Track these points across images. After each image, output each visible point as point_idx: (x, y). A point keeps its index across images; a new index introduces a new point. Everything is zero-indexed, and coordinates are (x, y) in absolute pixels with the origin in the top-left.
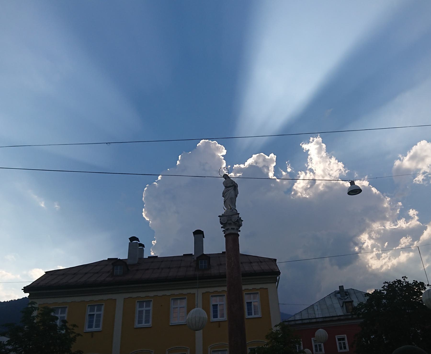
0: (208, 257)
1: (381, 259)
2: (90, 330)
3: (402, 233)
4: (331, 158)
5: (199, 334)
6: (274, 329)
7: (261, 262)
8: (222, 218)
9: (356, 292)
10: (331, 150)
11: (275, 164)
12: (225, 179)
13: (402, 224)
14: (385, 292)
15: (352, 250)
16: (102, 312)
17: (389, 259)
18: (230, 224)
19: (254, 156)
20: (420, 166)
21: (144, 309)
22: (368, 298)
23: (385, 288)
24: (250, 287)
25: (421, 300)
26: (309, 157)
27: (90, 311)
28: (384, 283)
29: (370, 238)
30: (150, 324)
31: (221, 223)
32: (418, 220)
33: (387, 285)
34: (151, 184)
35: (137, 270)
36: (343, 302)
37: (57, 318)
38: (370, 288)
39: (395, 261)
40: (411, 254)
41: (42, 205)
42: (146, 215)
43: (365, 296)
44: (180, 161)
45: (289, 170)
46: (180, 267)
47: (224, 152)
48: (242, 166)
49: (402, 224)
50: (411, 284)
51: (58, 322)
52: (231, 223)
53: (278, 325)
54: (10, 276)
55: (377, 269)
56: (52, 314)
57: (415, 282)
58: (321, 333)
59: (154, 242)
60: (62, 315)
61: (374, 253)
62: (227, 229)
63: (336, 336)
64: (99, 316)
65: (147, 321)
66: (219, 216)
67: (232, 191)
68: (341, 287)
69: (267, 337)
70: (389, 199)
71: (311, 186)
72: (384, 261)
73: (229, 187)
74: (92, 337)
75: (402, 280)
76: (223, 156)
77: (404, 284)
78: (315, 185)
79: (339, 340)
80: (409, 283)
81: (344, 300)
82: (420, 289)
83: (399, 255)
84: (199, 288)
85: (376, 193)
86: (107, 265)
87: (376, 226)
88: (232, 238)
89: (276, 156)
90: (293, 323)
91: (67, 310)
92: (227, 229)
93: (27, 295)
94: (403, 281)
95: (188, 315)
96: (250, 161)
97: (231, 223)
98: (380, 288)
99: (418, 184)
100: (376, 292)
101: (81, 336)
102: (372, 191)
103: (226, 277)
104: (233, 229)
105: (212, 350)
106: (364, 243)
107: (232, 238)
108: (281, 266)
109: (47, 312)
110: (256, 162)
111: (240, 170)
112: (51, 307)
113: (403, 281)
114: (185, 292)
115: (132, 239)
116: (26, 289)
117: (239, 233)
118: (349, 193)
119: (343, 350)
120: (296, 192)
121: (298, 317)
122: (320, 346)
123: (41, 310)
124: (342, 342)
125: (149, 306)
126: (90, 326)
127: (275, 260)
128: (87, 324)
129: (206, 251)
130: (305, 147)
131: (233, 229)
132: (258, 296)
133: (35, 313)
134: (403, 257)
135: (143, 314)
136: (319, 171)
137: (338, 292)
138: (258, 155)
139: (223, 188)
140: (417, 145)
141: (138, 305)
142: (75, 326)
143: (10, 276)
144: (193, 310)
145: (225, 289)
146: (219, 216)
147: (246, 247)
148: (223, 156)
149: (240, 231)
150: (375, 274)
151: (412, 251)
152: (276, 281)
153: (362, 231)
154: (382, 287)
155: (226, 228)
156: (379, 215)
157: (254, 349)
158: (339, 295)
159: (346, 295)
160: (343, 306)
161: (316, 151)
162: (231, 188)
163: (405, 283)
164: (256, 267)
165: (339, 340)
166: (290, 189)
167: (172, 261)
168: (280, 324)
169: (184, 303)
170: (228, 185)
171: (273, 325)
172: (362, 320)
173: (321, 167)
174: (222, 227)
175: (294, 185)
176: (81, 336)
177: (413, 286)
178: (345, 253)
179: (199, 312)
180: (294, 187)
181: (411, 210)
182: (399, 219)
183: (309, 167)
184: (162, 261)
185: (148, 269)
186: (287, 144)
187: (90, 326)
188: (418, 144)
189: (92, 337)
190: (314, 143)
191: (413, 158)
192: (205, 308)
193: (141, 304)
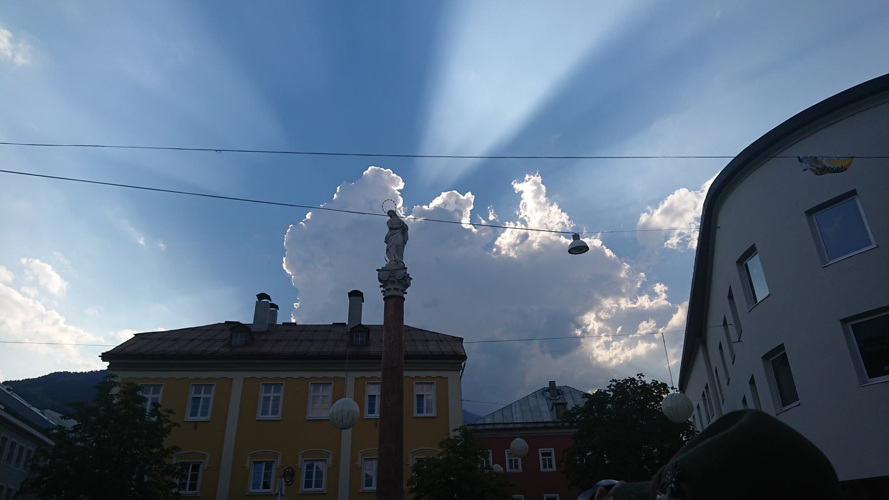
0: (367, 329)
2: (194, 419)
4: (551, 205)
6: (452, 435)
7: (441, 341)
9: (571, 390)
10: (553, 191)
11: (472, 207)
13: (644, 302)
14: (612, 393)
15: (572, 333)
16: (211, 396)
17: (623, 349)
18: (393, 282)
20: (674, 225)
21: (272, 395)
22: (586, 400)
24: (413, 374)
26: (522, 202)
27: (195, 393)
29: (598, 319)
30: (279, 416)
31: (380, 280)
32: (666, 299)
33: (615, 383)
34: (295, 223)
35: (266, 340)
37: (146, 400)
38: (593, 387)
39: (629, 353)
40: (653, 345)
41: (142, 242)
42: (287, 267)
44: (338, 194)
45: (491, 218)
46: (326, 340)
47: (401, 185)
48: (425, 207)
49: (644, 302)
51: (148, 407)
52: (395, 281)
54: (89, 337)
55: (605, 362)
56: (140, 393)
58: (519, 444)
59: (296, 305)
60: (154, 396)
61: (602, 341)
62: (388, 290)
64: (207, 400)
65: (275, 412)
67: (398, 235)
68: (552, 383)
69: (441, 445)
70: (627, 266)
71: (522, 242)
72: (615, 352)
75: (637, 378)
77: (639, 384)
78: (527, 242)
79: (543, 454)
83: (636, 344)
87: (608, 303)
88: (394, 304)
90: (481, 427)
91: (162, 389)
92: (388, 290)
93: (105, 366)
96: (437, 202)
97: (395, 281)
98: (604, 388)
101: (179, 426)
102: (605, 253)
104: (396, 289)
106: (588, 325)
107: (394, 304)
109: (131, 391)
110: (445, 203)
111: (423, 213)
112: (139, 384)
114: (434, 374)
115: (261, 296)
116: (105, 357)
117: (405, 296)
118: (570, 251)
119: (548, 470)
120: (499, 249)
122: (516, 461)
123: (124, 387)
124: (547, 458)
126: (194, 414)
127: (462, 339)
128: (189, 410)
129: (364, 322)
130: (518, 187)
131: (396, 289)
133: (115, 391)
134: (642, 348)
136: (534, 223)
137: (548, 390)
139: (386, 230)
141: (263, 389)
142: (170, 412)
143: (89, 337)
144: (338, 402)
145: (379, 374)
147: (413, 318)
150: (601, 369)
151: (655, 341)
153: (587, 309)
156: (613, 288)
158: (548, 394)
159: (559, 394)
161: (532, 195)
164: (433, 348)
165: (543, 454)
166: (491, 245)
168: (460, 428)
169: (329, 391)
170: (395, 226)
171: (451, 430)
173: (537, 216)
175: (496, 239)
176: (179, 426)
178: (563, 338)
179: (348, 404)
180: (497, 243)
181: (658, 285)
182: (641, 295)
183: (520, 217)
185: (281, 340)
186: (491, 182)
187: (194, 414)
188: (676, 192)
190: (530, 182)
191: (667, 212)
192: (358, 399)
193: (268, 387)
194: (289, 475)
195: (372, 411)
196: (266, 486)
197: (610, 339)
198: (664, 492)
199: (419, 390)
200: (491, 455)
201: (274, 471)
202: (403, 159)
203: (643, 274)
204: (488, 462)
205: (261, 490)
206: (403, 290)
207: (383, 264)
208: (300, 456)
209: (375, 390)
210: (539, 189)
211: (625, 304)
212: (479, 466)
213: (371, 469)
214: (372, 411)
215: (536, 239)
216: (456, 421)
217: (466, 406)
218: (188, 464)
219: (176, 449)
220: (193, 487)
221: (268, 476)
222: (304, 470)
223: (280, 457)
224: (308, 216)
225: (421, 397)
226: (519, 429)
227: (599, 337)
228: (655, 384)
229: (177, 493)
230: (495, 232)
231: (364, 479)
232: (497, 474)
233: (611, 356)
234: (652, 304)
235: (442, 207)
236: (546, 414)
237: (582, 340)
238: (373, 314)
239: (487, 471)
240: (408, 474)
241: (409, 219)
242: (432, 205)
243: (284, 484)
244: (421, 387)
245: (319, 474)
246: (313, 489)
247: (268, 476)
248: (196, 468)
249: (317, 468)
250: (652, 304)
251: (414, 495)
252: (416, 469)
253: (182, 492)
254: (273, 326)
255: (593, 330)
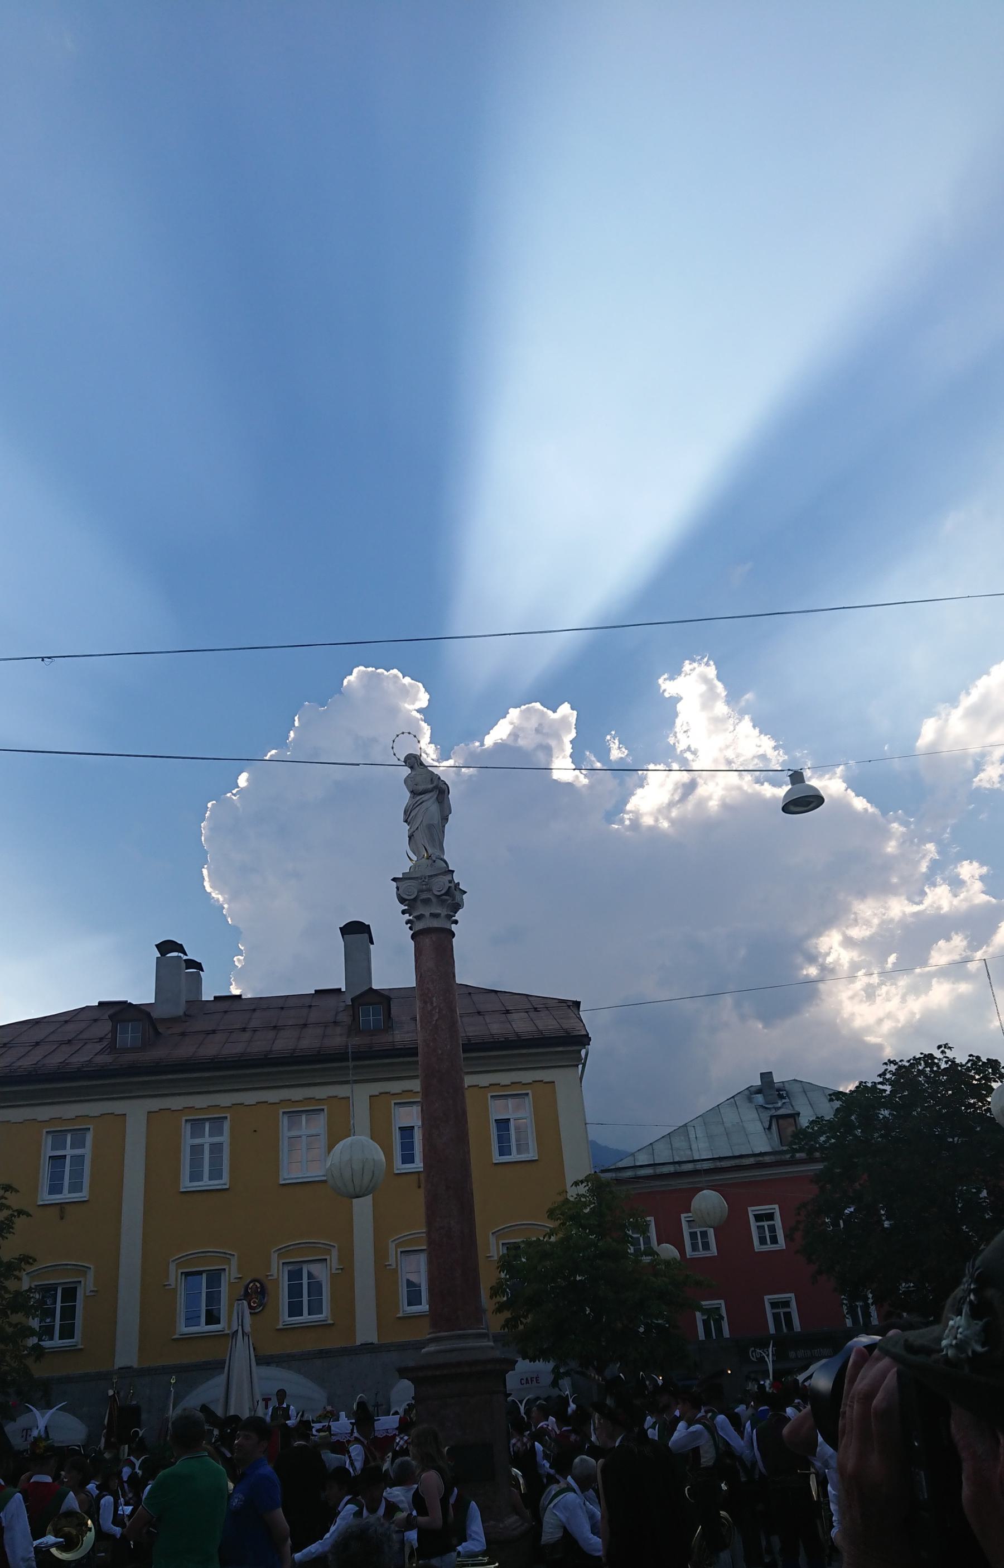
0: (383, 999)
1: (878, 1000)
2: (57, 1198)
3: (939, 927)
5: (363, 1209)
6: (572, 1193)
7: (536, 1009)
8: (400, 884)
9: (807, 1088)
11: (573, 734)
12: (412, 768)
13: (940, 898)
16: (87, 1151)
17: (904, 999)
18: (427, 902)
19: (511, 710)
21: (207, 1140)
22: (837, 1104)
23: (888, 1076)
24: (484, 1080)
25: (989, 1110)
26: (678, 722)
27: (54, 1148)
28: (886, 1064)
29: (848, 942)
30: (224, 1181)
31: (402, 900)
35: (183, 1034)
36: (772, 1117)
38: (849, 1079)
39: (916, 1006)
40: (964, 988)
43: (831, 1100)
46: (305, 1025)
47: (423, 699)
49: (940, 898)
50: (962, 1066)
52: (432, 900)
53: (582, 1182)
55: (868, 1030)
57: (975, 1061)
58: (709, 1201)
59: (238, 961)
62: (419, 918)
63: (750, 1209)
64: (78, 1160)
66: (394, 880)
69: (551, 1214)
73: (421, 794)
74: (62, 1218)
75: (937, 1054)
76: (419, 711)
77: (943, 1066)
78: (692, 799)
79: (758, 1218)
80: (957, 1061)
81: (773, 1112)
82: (989, 1080)
83: (929, 987)
84: (356, 1082)
85: (866, 810)
86: (95, 1020)
88: (434, 944)
89: (575, 712)
90: (629, 1174)
92: (419, 918)
94: (941, 1056)
95: (332, 1153)
96: (500, 733)
97: (432, 900)
98: (871, 1078)
99: (986, 789)
100: (862, 1088)
101: (28, 1215)
103: (416, 1055)
105: (399, 1250)
106: (828, 954)
107: (434, 944)
108: (591, 1020)
110: (514, 735)
113: (941, 1056)
115: (166, 947)
117: (454, 927)
118: (786, 809)
119: (769, 1247)
121: (643, 1159)
122: (704, 1234)
124: (765, 1224)
125: (221, 1134)
127: (577, 1004)
128: (45, 1182)
129: (375, 986)
130: (669, 687)
132: (528, 1102)
134: (940, 994)
135: (63, 1179)
137: (759, 1091)
138: (523, 707)
140: (988, 673)
141: (187, 1129)
144: (342, 1143)
145: (416, 1085)
146: (394, 880)
147: (475, 965)
148: (419, 711)
149: (456, 922)
150: (856, 1045)
151: (967, 977)
152: (577, 1061)
153: (827, 923)
154: (880, 1076)
155: (415, 914)
156: (874, 877)
157: (516, 1247)
158: (760, 1099)
159: (781, 1097)
160: (770, 1128)
162: (431, 794)
163: (946, 1062)
164: (521, 1025)
165: (758, 1218)
167: (282, 1008)
168: (587, 1179)
169: (319, 1125)
170: (421, 788)
171: (569, 1180)
172: (820, 1166)
173: (712, 745)
174: (404, 912)
176: (28, 1215)
177: (969, 1070)
178: (781, 984)
179: (360, 1148)
184: (254, 1010)
185: (214, 1032)
186: (610, 678)
187: (55, 1188)
189: (62, 1218)
191: (975, 712)
192: (379, 1134)
193: (197, 1125)
194: (256, 1294)
195: (408, 1158)
196: (212, 1318)
197: (875, 979)
198: (959, 1313)
199: (498, 1110)
200: (653, 1224)
201: (224, 1288)
202: (418, 641)
203: (931, 847)
204: (647, 1241)
205: (204, 1328)
206: (449, 917)
207: (403, 867)
208: (274, 1257)
209: (411, 1116)
210: (712, 688)
211: (899, 908)
212: (631, 1250)
213: (416, 1270)
214: (408, 1158)
215: (715, 791)
216: (577, 1167)
217: (594, 1133)
218: (54, 1288)
219: (27, 1259)
220: (67, 1332)
221: (213, 1298)
222: (285, 1283)
223: (234, 1262)
224: (243, 780)
225: (503, 1124)
226: (708, 1172)
227: (852, 978)
228: (974, 1063)
229: (37, 1347)
230: (622, 783)
231: (403, 1291)
232: (667, 1263)
233: (881, 1014)
234: (956, 902)
235: (510, 742)
236: (757, 1138)
237: (821, 986)
238: (394, 967)
239: (646, 1259)
240: (489, 1276)
241: (444, 768)
242: (489, 741)
243: (247, 1312)
244: (500, 1103)
245: (315, 1288)
246: (306, 1317)
247: (213, 1298)
248: (70, 1294)
249: (310, 1275)
250: (956, 902)
251: (507, 1314)
252: (506, 1264)
253: (47, 1344)
254: (196, 1007)
255: (837, 961)
